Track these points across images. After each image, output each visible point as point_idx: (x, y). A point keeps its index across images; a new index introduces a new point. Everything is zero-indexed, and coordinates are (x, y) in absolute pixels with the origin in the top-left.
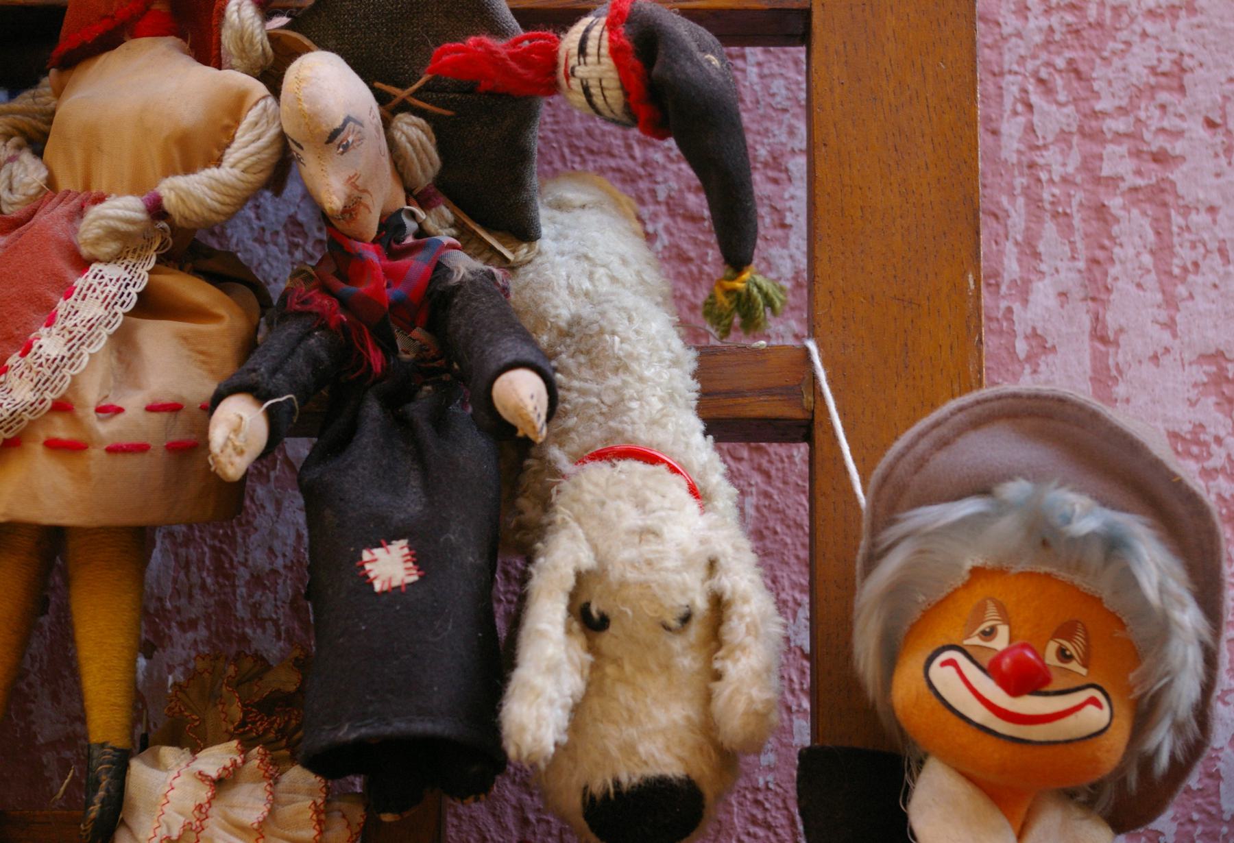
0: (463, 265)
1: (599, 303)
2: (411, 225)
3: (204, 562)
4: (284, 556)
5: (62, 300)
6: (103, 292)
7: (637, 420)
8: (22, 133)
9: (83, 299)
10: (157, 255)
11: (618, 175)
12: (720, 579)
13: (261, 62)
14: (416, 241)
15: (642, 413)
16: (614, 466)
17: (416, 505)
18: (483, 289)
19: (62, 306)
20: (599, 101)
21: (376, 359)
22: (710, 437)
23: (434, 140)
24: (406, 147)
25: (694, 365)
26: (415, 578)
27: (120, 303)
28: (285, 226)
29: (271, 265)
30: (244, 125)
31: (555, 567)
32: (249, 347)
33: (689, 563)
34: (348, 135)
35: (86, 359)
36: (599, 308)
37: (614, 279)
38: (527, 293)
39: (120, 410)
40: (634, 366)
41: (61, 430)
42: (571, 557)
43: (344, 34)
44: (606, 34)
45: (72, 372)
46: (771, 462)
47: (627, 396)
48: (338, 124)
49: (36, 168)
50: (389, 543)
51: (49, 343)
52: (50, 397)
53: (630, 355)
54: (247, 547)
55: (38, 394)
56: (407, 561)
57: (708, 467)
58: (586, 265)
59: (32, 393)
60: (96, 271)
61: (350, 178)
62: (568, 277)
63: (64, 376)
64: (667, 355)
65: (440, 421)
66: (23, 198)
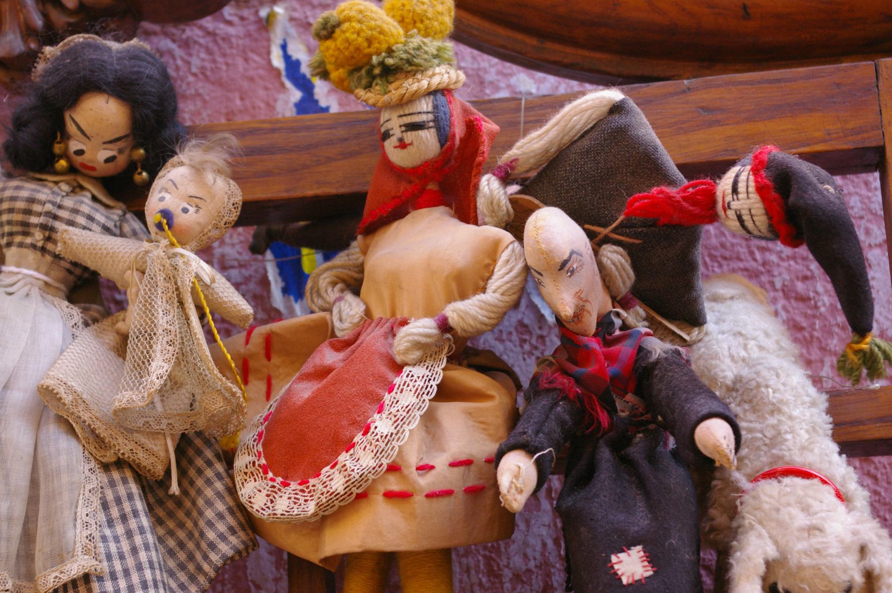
0: (658, 347)
1: (754, 366)
2: (618, 322)
3: (479, 567)
4: (535, 559)
5: (387, 394)
6: (414, 386)
7: (792, 447)
8: (343, 281)
9: (401, 392)
10: (447, 357)
11: (745, 273)
12: (870, 560)
13: (506, 218)
14: (622, 332)
15: (795, 442)
16: (779, 482)
17: (644, 520)
18: (675, 362)
19: (387, 398)
20: (749, 224)
21: (603, 417)
22: (844, 456)
23: (629, 261)
24: (611, 269)
25: (826, 405)
26: (651, 573)
27: (426, 393)
28: (516, 328)
29: (509, 356)
30: (500, 263)
31: (749, 559)
32: (514, 418)
33: (846, 550)
34: (573, 263)
35: (407, 434)
36: (754, 369)
37: (761, 348)
38: (701, 362)
39: (432, 468)
40: (785, 409)
41: (394, 484)
42: (760, 551)
43: (561, 193)
44: (752, 178)
45: (398, 443)
46: (876, 468)
47: (783, 431)
48: (566, 257)
49: (357, 305)
50: (630, 549)
51: (382, 425)
52: (385, 462)
53: (781, 401)
54: (508, 554)
55: (377, 461)
56: (643, 561)
57: (847, 477)
58: (741, 339)
59: (374, 460)
60: (408, 372)
61: (577, 293)
62: (729, 349)
63: (394, 447)
64: (807, 399)
65: (652, 458)
66: (350, 325)
